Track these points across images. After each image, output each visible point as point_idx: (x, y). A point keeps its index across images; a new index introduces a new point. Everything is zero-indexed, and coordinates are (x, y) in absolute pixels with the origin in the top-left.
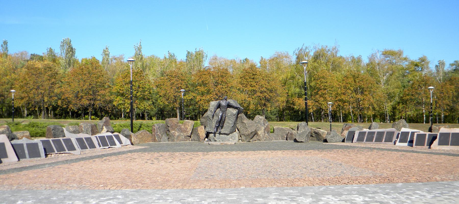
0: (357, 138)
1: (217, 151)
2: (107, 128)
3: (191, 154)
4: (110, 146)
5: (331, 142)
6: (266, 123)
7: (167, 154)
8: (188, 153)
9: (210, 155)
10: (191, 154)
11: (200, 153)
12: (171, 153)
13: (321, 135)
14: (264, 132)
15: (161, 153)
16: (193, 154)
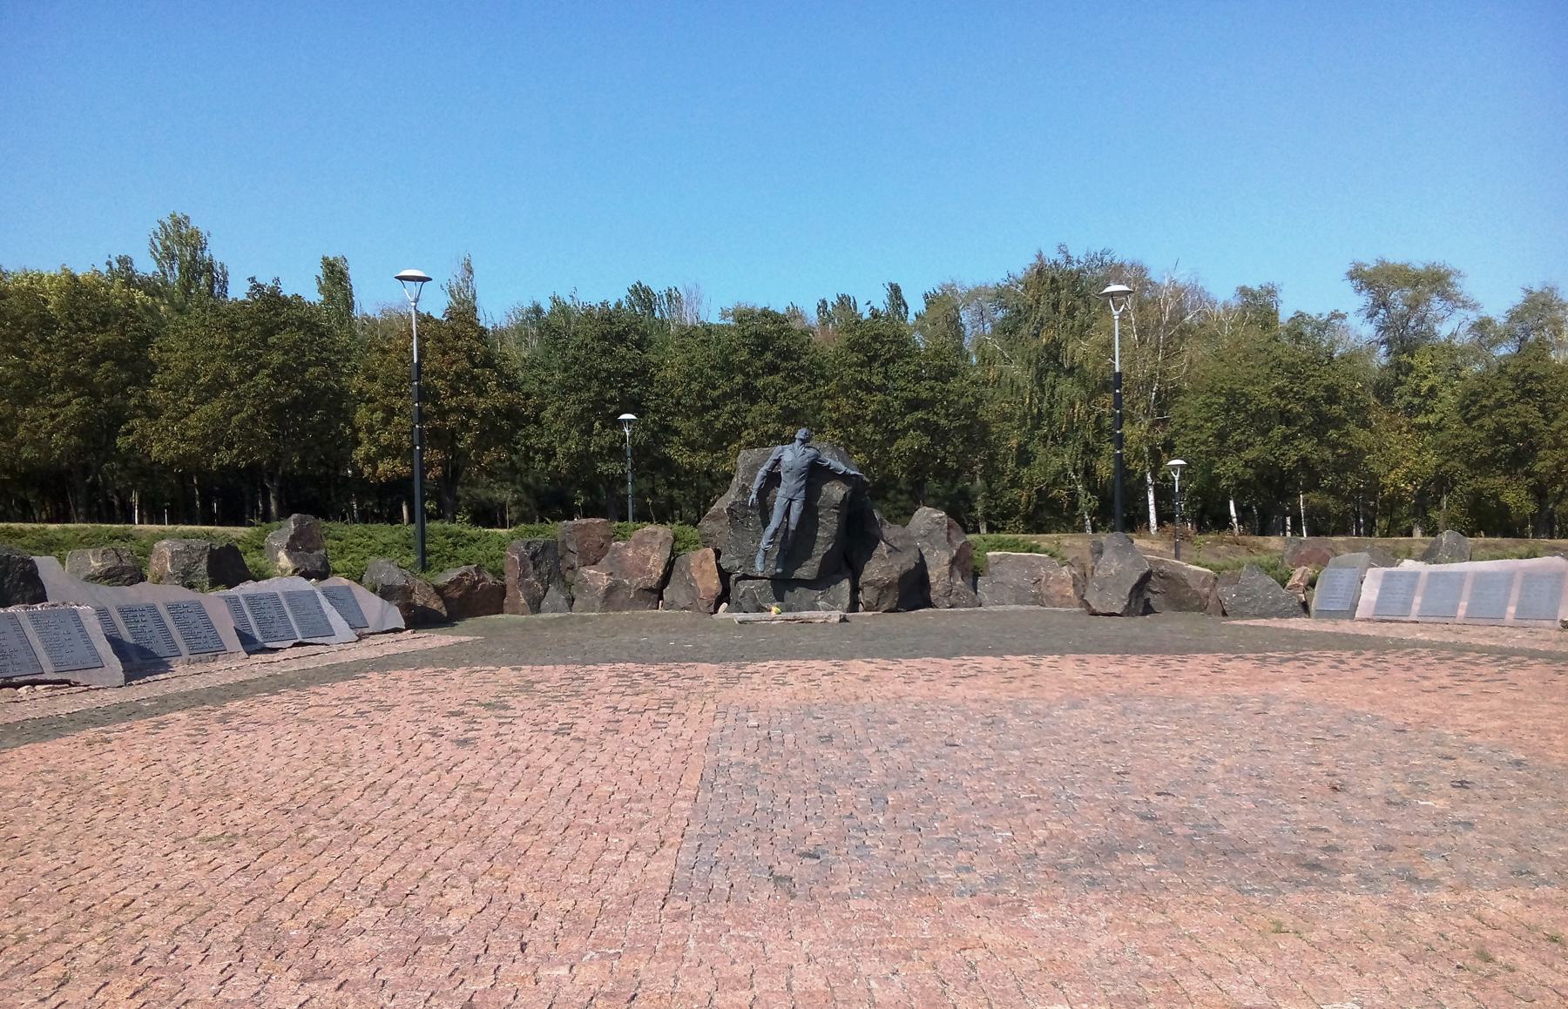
0: (1374, 598)
1: (785, 658)
2: (295, 561)
3: (666, 676)
4: (300, 639)
5: (1242, 616)
6: (958, 538)
7: (557, 675)
8: (651, 670)
9: (756, 678)
10: (666, 676)
11: (706, 669)
12: (571, 667)
13: (1187, 586)
14: (951, 574)
15: (526, 669)
16: (678, 676)
